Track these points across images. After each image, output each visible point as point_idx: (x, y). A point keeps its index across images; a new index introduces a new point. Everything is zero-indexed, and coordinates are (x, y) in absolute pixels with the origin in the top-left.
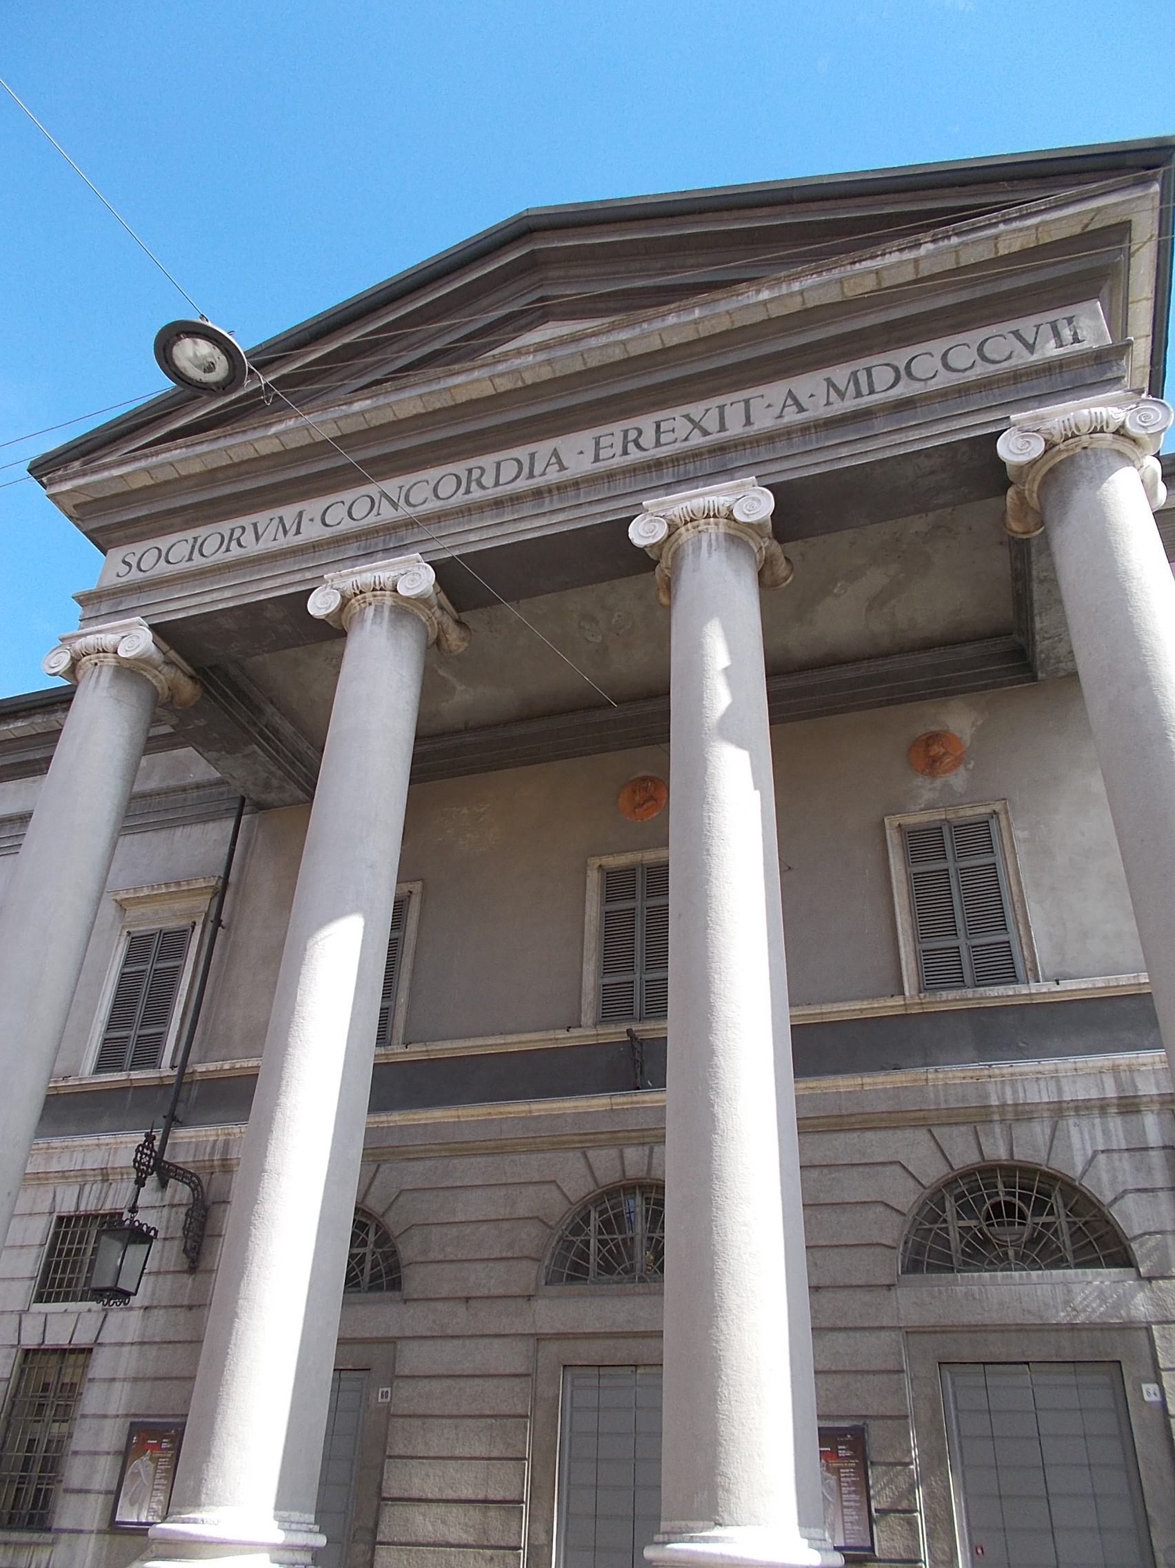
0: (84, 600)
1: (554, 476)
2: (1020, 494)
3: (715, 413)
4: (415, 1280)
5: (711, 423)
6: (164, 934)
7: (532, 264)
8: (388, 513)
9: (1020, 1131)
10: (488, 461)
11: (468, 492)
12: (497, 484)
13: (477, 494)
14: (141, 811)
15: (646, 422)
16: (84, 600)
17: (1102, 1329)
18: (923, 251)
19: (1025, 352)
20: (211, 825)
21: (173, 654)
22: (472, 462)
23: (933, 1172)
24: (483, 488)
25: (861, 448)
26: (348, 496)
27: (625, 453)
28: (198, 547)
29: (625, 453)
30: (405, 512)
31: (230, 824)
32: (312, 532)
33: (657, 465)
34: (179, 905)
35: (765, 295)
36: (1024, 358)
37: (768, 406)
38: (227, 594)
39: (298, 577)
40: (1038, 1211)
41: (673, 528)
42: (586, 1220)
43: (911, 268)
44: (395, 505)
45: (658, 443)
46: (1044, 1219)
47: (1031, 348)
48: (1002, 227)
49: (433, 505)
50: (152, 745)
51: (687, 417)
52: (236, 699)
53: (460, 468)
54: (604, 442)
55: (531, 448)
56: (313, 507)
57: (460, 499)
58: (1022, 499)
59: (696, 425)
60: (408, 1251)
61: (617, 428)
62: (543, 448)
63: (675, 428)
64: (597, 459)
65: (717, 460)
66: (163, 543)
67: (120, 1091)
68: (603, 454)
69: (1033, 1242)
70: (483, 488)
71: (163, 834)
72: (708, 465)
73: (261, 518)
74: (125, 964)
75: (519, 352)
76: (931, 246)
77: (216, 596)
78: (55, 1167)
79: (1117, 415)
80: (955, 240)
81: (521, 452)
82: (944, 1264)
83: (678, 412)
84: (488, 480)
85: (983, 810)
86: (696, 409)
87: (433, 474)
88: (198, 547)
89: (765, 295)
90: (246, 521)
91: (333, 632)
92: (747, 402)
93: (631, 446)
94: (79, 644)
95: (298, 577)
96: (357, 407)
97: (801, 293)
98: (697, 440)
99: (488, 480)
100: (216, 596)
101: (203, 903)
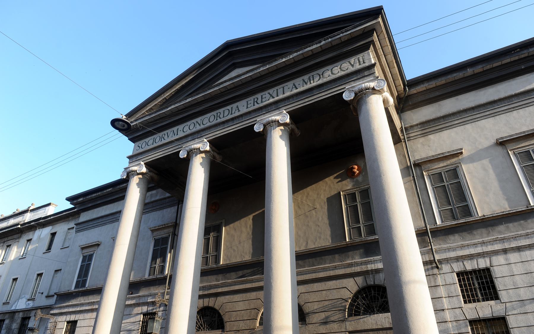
0: (129, 157)
1: (237, 114)
2: (353, 106)
3: (276, 92)
4: (228, 326)
5: (274, 94)
6: (163, 238)
7: (230, 55)
8: (198, 128)
9: (377, 276)
10: (221, 110)
11: (217, 120)
12: (224, 117)
13: (219, 120)
14: (147, 207)
15: (259, 96)
16: (129, 157)
17: (41, 309)
18: (322, 44)
19: (351, 68)
20: (172, 208)
21: (151, 169)
22: (218, 111)
23: (355, 289)
24: (220, 118)
25: (311, 98)
26: (188, 123)
27: (254, 105)
28: (154, 141)
29: (254, 105)
30: (202, 127)
31: (176, 207)
32: (181, 134)
33: (261, 109)
34: (166, 231)
35: (284, 60)
36: (351, 69)
37: (288, 90)
38: (161, 153)
39: (177, 147)
40: (382, 298)
41: (265, 126)
42: (358, 298)
43: (320, 48)
44: (200, 125)
45: (262, 102)
46: (383, 300)
47: (353, 66)
48: (341, 35)
49: (209, 124)
50: (149, 189)
51: (269, 93)
52: (166, 179)
53: (214, 113)
54: (249, 102)
55: (232, 106)
56: (180, 127)
57: (215, 122)
58: (353, 106)
59: (271, 95)
60: (226, 318)
61: (252, 98)
62: (234, 106)
63: (267, 97)
64: (247, 108)
65: (276, 106)
66: (147, 140)
67: (79, 292)
68: (249, 106)
69: (380, 307)
70: (220, 118)
71: (161, 211)
72: (273, 107)
73: (168, 131)
74: (154, 247)
75: (225, 82)
76: (324, 42)
77: (159, 154)
78: (141, 301)
79: (372, 85)
80: (330, 40)
81: (229, 107)
82: (357, 314)
83: (266, 92)
84: (221, 116)
85: (366, 186)
86: (271, 91)
87: (208, 115)
88: (154, 141)
89: (284, 60)
90: (165, 132)
91: (187, 161)
92: (283, 88)
93: (255, 103)
94: (128, 170)
95: (177, 147)
96: (188, 100)
97: (293, 58)
98: (272, 100)
99: (221, 116)
100: (159, 154)
101: (171, 230)
